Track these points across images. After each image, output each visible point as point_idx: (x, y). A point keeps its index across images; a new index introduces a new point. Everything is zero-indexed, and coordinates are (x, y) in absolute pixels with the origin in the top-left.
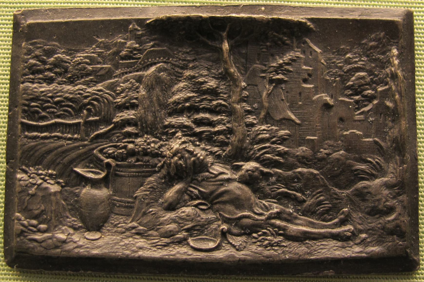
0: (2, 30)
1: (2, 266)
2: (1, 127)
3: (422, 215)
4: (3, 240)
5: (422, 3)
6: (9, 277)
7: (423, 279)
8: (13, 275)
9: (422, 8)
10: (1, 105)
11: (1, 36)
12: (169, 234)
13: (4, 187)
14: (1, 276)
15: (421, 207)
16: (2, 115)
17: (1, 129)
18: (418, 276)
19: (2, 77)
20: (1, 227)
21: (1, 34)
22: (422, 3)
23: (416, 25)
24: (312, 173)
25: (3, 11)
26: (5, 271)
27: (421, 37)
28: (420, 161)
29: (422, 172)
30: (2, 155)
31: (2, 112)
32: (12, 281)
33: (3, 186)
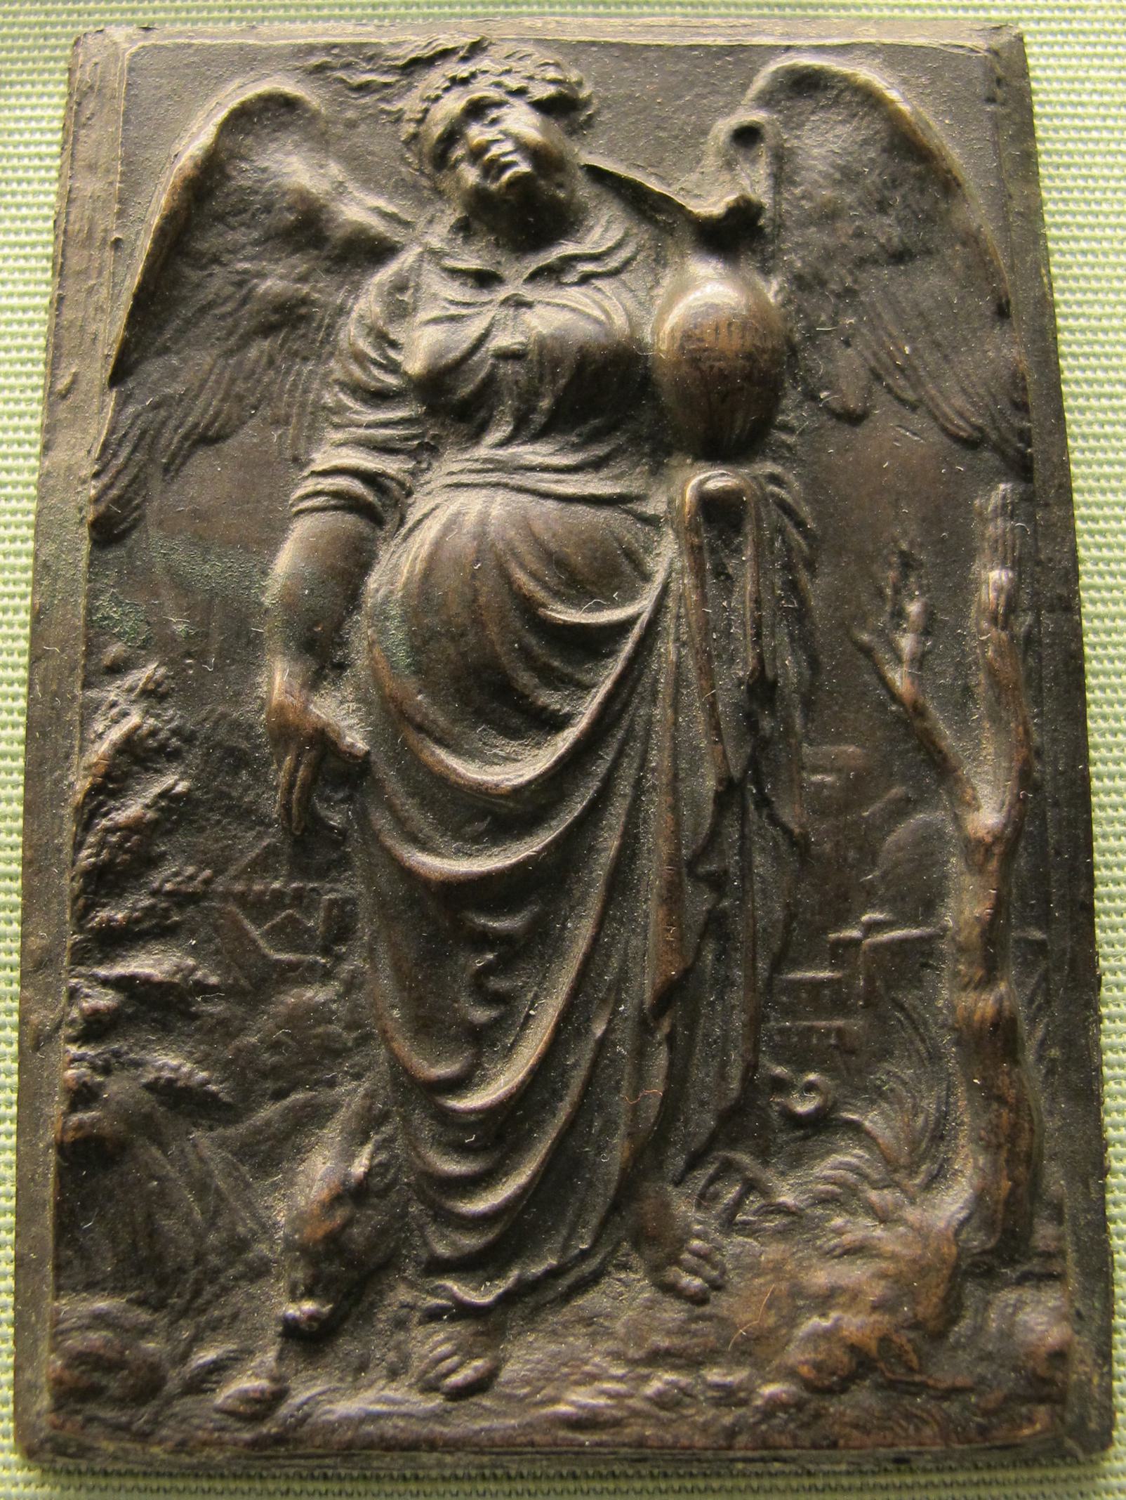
0: (4, 176)
3: (1121, 1142)
4: (10, 1300)
5: (1122, 8)
7: (1124, 1050)
9: (1119, 356)
10: (1, 540)
11: (1, 540)
13: (11, 1425)
14: (6, 1474)
15: (1118, 1194)
19: (5, 421)
20: (4, 1316)
21: (2, 328)
22: (1122, 8)
23: (1097, 794)
24: (872, 800)
25: (8, 73)
26: (21, 1486)
27: (1114, 491)
28: (1110, 1130)
33: (5, 1356)
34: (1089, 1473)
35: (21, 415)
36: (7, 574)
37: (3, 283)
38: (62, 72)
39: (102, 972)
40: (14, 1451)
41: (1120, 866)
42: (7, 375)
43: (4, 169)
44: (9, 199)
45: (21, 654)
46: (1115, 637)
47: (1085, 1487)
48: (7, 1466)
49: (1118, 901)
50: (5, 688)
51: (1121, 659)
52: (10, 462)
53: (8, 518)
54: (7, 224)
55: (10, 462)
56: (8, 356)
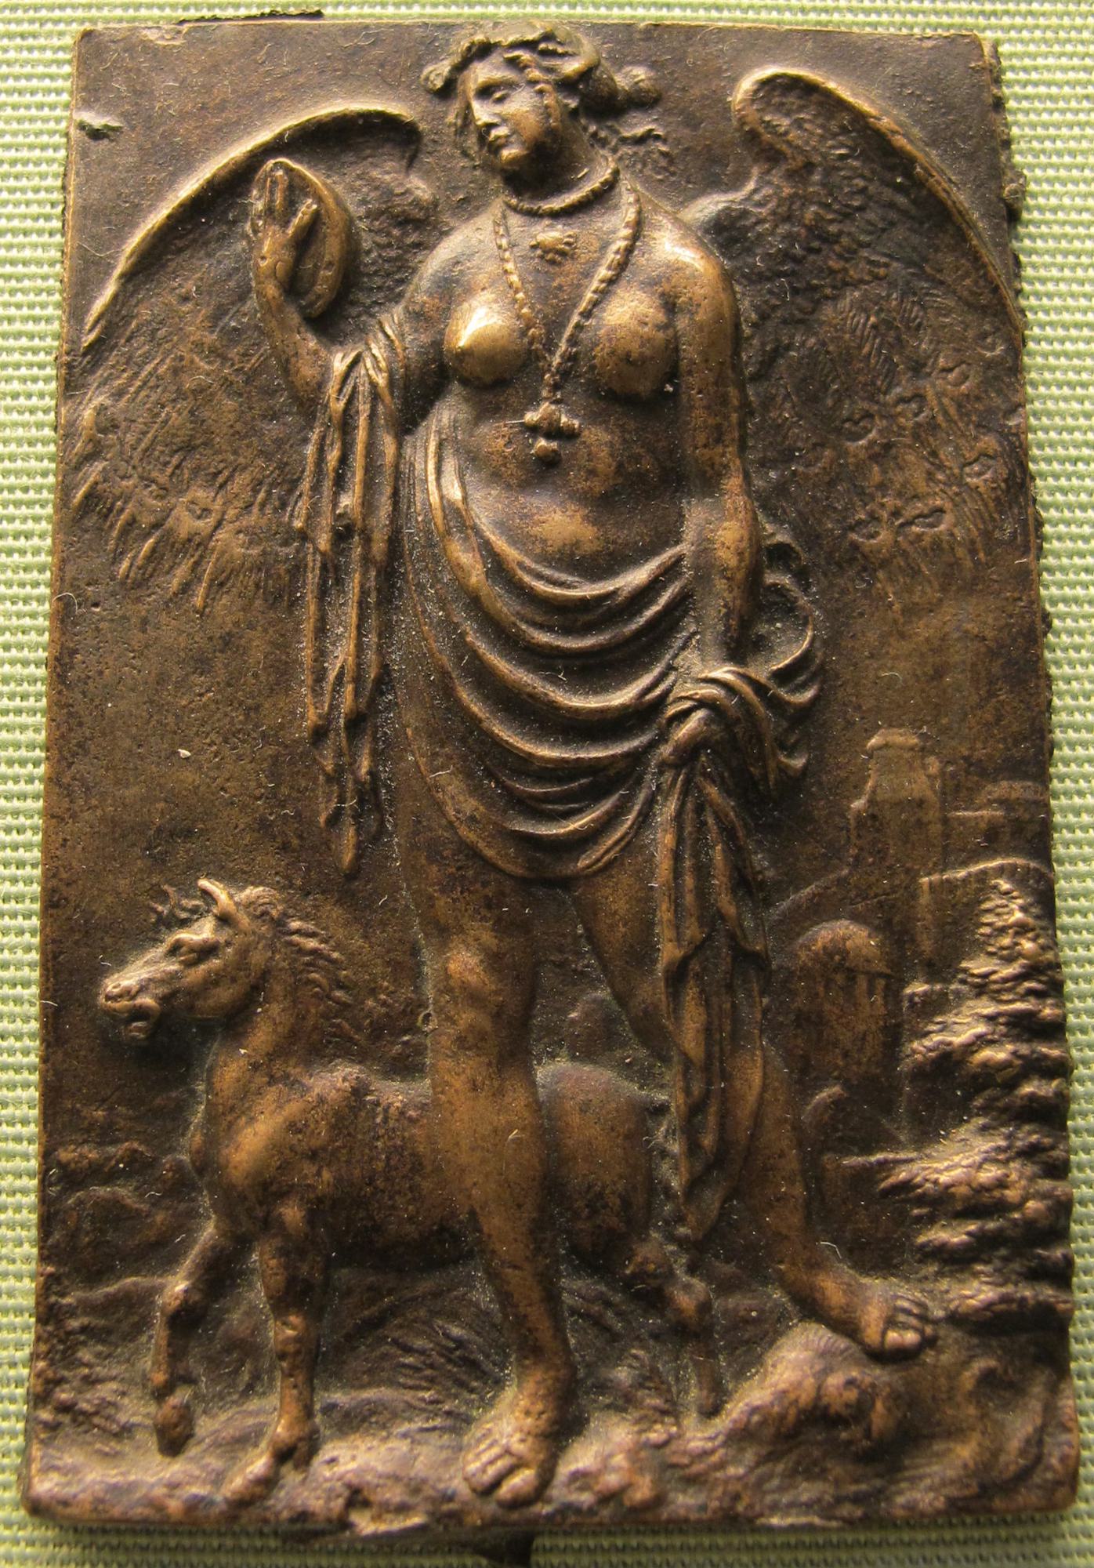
1: (8, 1525)
2: (7, 1382)
3: (1088, 1305)
6: (18, 1284)
7: (1090, 1339)
8: (31, 1543)
12: (386, 1409)
14: (7, 1533)
16: (8, 604)
17: (5, 1320)
18: (1073, 1543)
29: (1085, 1245)
30: (7, 1438)
31: (6, 689)
32: (30, 1564)
34: (1045, 1532)
35: (23, 763)
36: (9, 574)
37: (4, 965)
38: (56, 176)
39: (87, 327)
40: (16, 1506)
41: (1086, 894)
42: (10, 763)
43: (5, 505)
44: (9, 111)
45: (36, 797)
46: (1080, 751)
47: (1041, 1547)
48: (8, 1525)
49: (1087, 967)
50: (6, 990)
51: (1090, 728)
52: (11, 718)
53: (9, 820)
54: (8, 139)
55: (11, 718)
56: (10, 592)
